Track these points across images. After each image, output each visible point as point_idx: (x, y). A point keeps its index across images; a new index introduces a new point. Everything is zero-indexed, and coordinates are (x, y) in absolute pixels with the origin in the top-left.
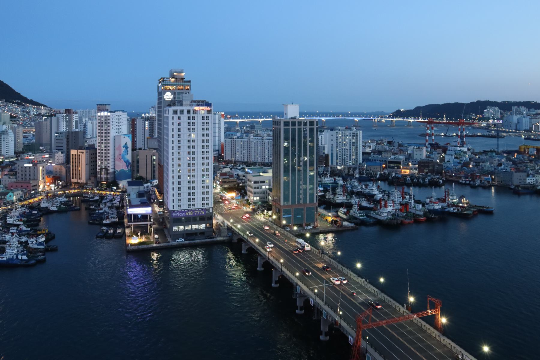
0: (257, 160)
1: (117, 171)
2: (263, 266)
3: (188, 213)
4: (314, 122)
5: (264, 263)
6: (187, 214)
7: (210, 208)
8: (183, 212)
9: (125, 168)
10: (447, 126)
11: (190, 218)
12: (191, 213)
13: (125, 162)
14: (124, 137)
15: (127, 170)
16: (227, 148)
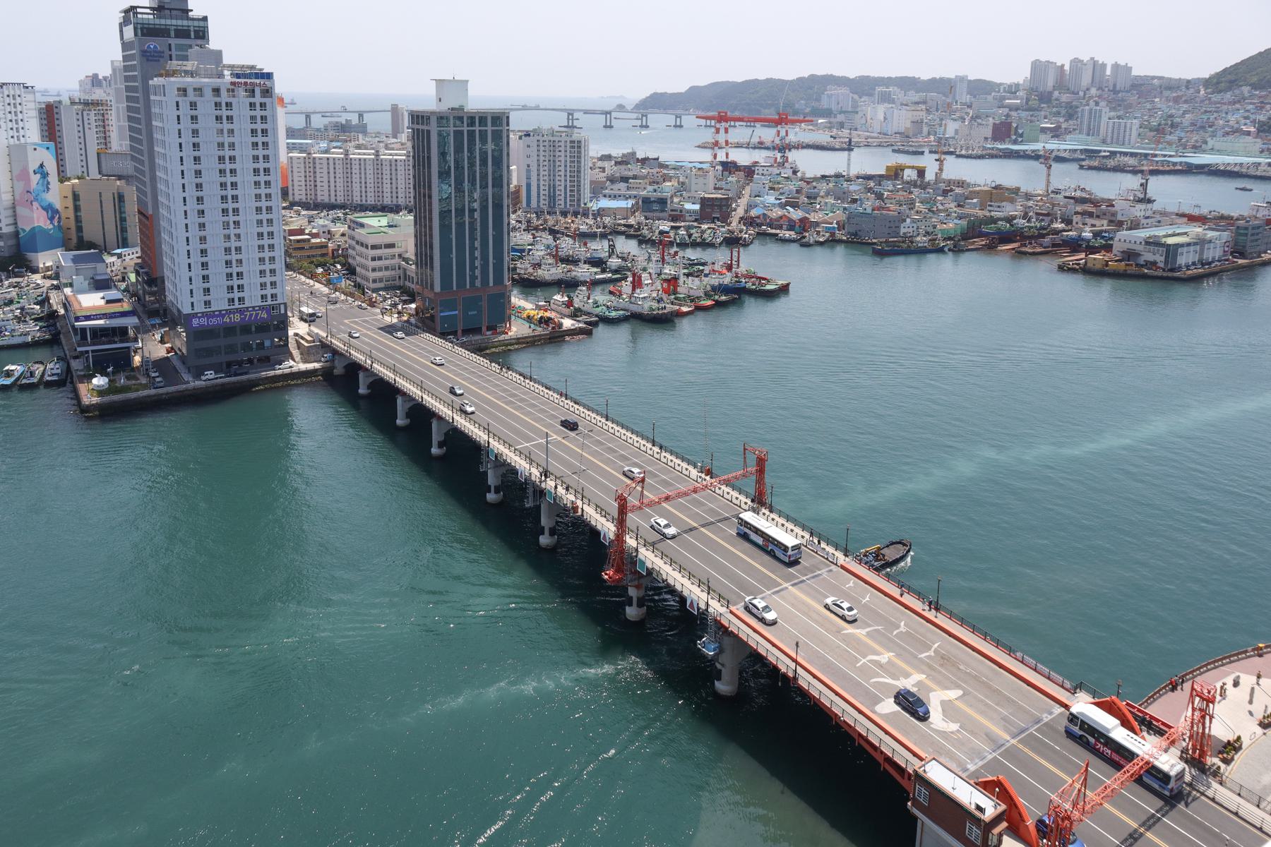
0: (366, 201)
1: (24, 230)
2: (408, 415)
3: (230, 318)
4: (486, 118)
5: (409, 408)
6: (228, 320)
7: (279, 304)
8: (217, 316)
9: (45, 222)
10: (750, 126)
11: (235, 327)
12: (237, 318)
13: (44, 209)
14: (35, 149)
15: (51, 226)
16: (295, 174)
